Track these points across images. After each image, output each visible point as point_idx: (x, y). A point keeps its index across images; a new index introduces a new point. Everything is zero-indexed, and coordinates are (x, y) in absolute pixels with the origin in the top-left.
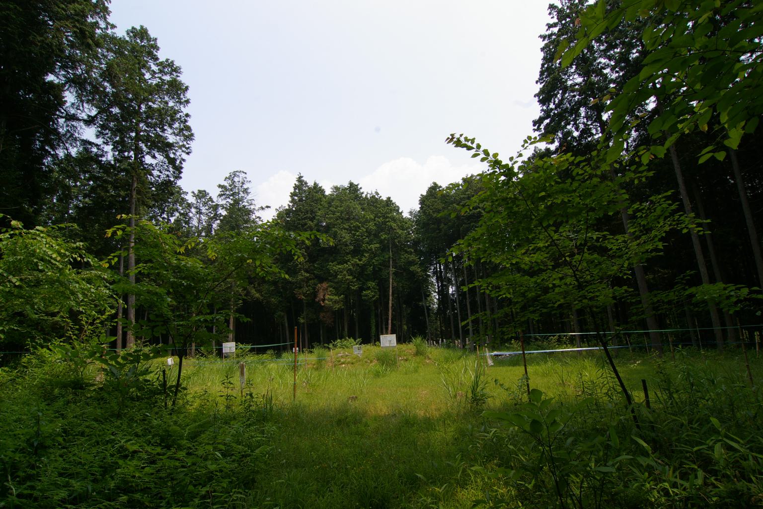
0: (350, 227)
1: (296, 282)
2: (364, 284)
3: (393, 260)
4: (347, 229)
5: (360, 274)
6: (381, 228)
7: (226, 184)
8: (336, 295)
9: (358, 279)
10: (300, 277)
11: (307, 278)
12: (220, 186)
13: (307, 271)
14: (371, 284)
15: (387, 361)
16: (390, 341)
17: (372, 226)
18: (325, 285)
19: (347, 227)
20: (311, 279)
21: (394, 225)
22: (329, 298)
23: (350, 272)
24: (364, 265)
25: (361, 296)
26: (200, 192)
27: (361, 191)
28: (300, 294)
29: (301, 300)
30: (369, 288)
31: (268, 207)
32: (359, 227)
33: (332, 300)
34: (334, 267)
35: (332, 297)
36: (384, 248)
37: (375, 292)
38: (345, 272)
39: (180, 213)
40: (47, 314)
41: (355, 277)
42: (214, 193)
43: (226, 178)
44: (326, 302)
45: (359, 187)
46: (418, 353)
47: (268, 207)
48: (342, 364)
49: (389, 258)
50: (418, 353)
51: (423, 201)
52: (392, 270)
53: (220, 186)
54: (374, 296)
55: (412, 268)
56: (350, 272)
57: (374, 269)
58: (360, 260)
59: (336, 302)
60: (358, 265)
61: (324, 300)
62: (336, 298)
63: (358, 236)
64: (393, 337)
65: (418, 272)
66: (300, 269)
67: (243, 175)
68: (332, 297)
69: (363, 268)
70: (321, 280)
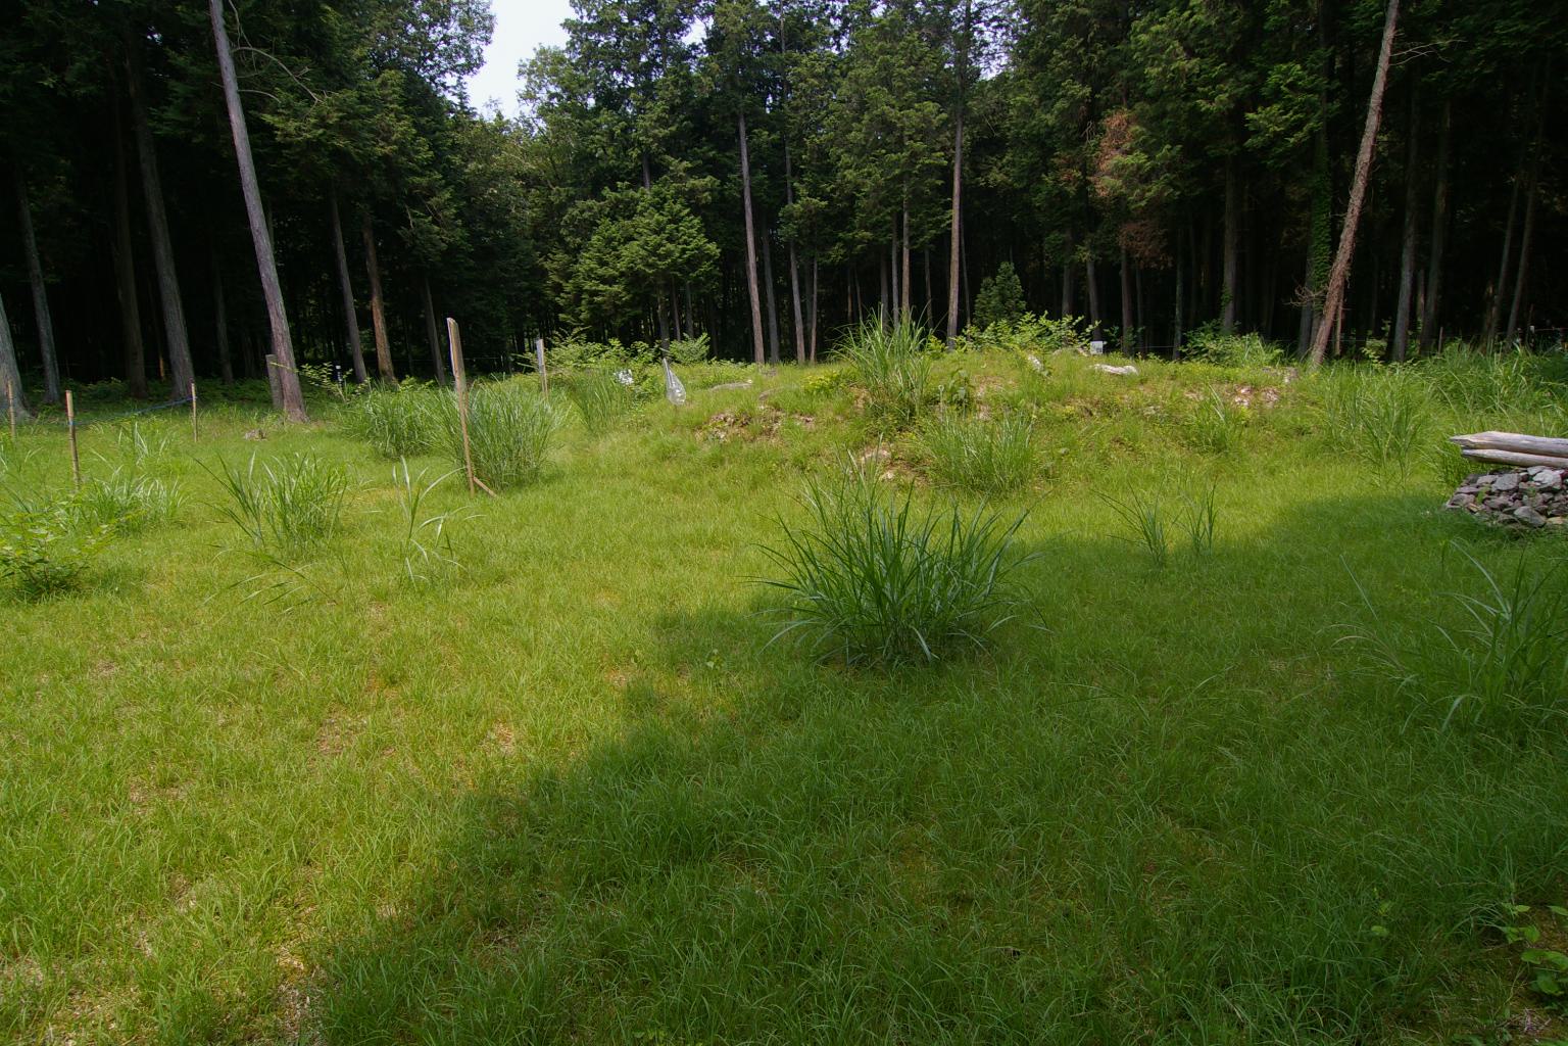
40: (604, 280)
54: (1297, 126)
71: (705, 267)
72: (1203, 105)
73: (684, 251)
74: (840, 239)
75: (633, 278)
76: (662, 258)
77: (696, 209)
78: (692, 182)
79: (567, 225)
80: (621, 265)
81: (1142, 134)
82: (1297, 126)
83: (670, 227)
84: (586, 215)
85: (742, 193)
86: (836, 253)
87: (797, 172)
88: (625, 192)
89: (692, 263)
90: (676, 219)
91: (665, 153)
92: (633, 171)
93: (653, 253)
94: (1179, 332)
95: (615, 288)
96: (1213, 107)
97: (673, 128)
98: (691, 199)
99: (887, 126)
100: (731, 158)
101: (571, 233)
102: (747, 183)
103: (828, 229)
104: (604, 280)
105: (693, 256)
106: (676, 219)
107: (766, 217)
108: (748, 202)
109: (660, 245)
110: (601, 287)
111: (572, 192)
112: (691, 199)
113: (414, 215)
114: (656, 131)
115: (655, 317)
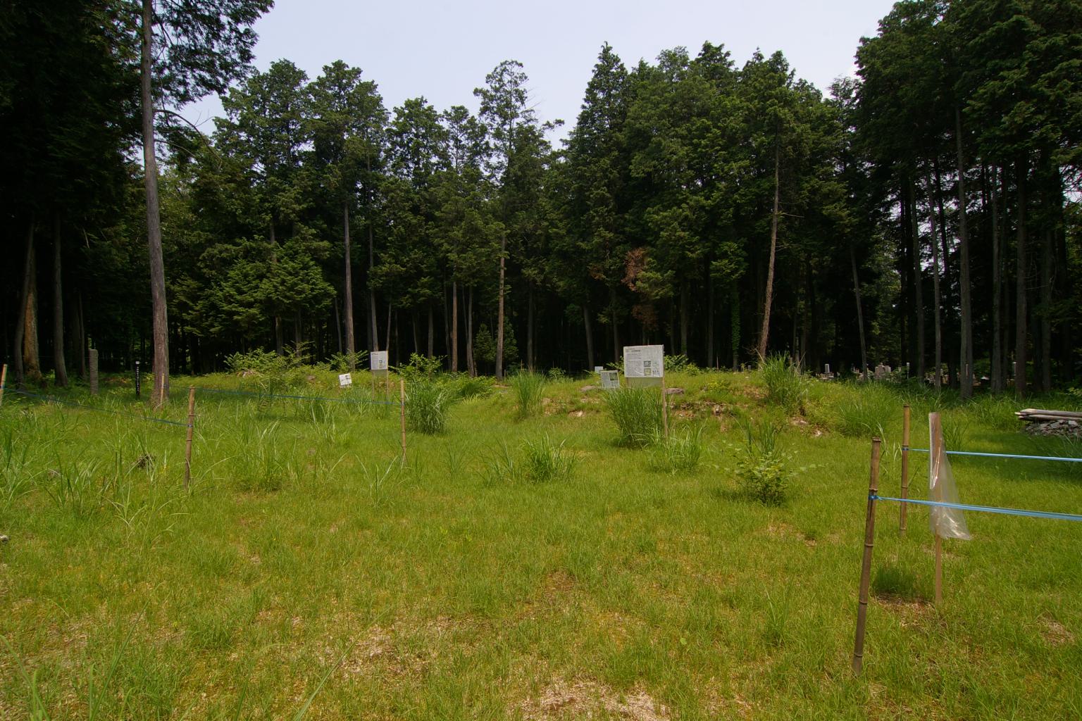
0: (689, 131)
1: (591, 250)
2: (715, 246)
3: (781, 192)
4: (682, 137)
5: (708, 226)
6: (754, 121)
7: (487, 87)
8: (657, 271)
9: (704, 238)
10: (596, 240)
11: (610, 240)
12: (476, 92)
13: (607, 228)
14: (730, 246)
15: (634, 425)
16: (647, 364)
17: (735, 123)
18: (639, 252)
19: (685, 132)
20: (619, 243)
21: (784, 112)
22: (644, 275)
23: (686, 223)
24: (717, 206)
25: (708, 271)
26: (457, 110)
27: (729, 59)
28: (598, 271)
29: (600, 282)
30: (724, 255)
31: (560, 122)
32: (707, 129)
33: (649, 279)
34: (655, 215)
35: (649, 274)
36: (763, 164)
37: (738, 263)
38: (675, 224)
39: (245, 78)
40: (242, 304)
41: (696, 233)
42: (474, 107)
43: (489, 77)
44: (639, 283)
45: (724, 51)
46: (776, 398)
47: (560, 122)
48: (578, 409)
49: (773, 188)
50: (776, 398)
51: (868, 53)
52: (777, 214)
53: (476, 92)
54: (735, 271)
55: (828, 209)
56: (686, 223)
57: (736, 215)
58: (707, 198)
59: (657, 284)
60: (703, 207)
61: (634, 281)
62: (658, 275)
63: (706, 146)
64: (655, 353)
65: (841, 218)
66: (598, 225)
67: (516, 69)
68: (649, 274)
69: (714, 213)
70: (637, 242)
71: (327, 302)
72: (690, 255)
73: (312, 290)
74: (408, 293)
75: (268, 305)
76: (299, 293)
77: (319, 261)
78: (315, 244)
79: (204, 260)
80: (259, 295)
81: (654, 263)
82: (735, 271)
83: (302, 273)
84: (224, 255)
85: (344, 255)
86: (405, 301)
87: (383, 248)
88: (258, 242)
89: (317, 299)
90: (306, 267)
91: (299, 221)
92: (264, 229)
93: (291, 289)
94: (864, 352)
95: (253, 311)
96: (694, 256)
97: (305, 206)
98: (314, 254)
99: (474, 230)
100: (336, 231)
101: (206, 266)
102: (348, 249)
103: (402, 285)
104: (242, 304)
105: (319, 293)
106: (306, 267)
107: (360, 277)
108: (348, 261)
109: (296, 284)
110: (241, 309)
111: (211, 237)
112: (314, 254)
113: (89, 237)
114: (295, 206)
115: (902, 328)
